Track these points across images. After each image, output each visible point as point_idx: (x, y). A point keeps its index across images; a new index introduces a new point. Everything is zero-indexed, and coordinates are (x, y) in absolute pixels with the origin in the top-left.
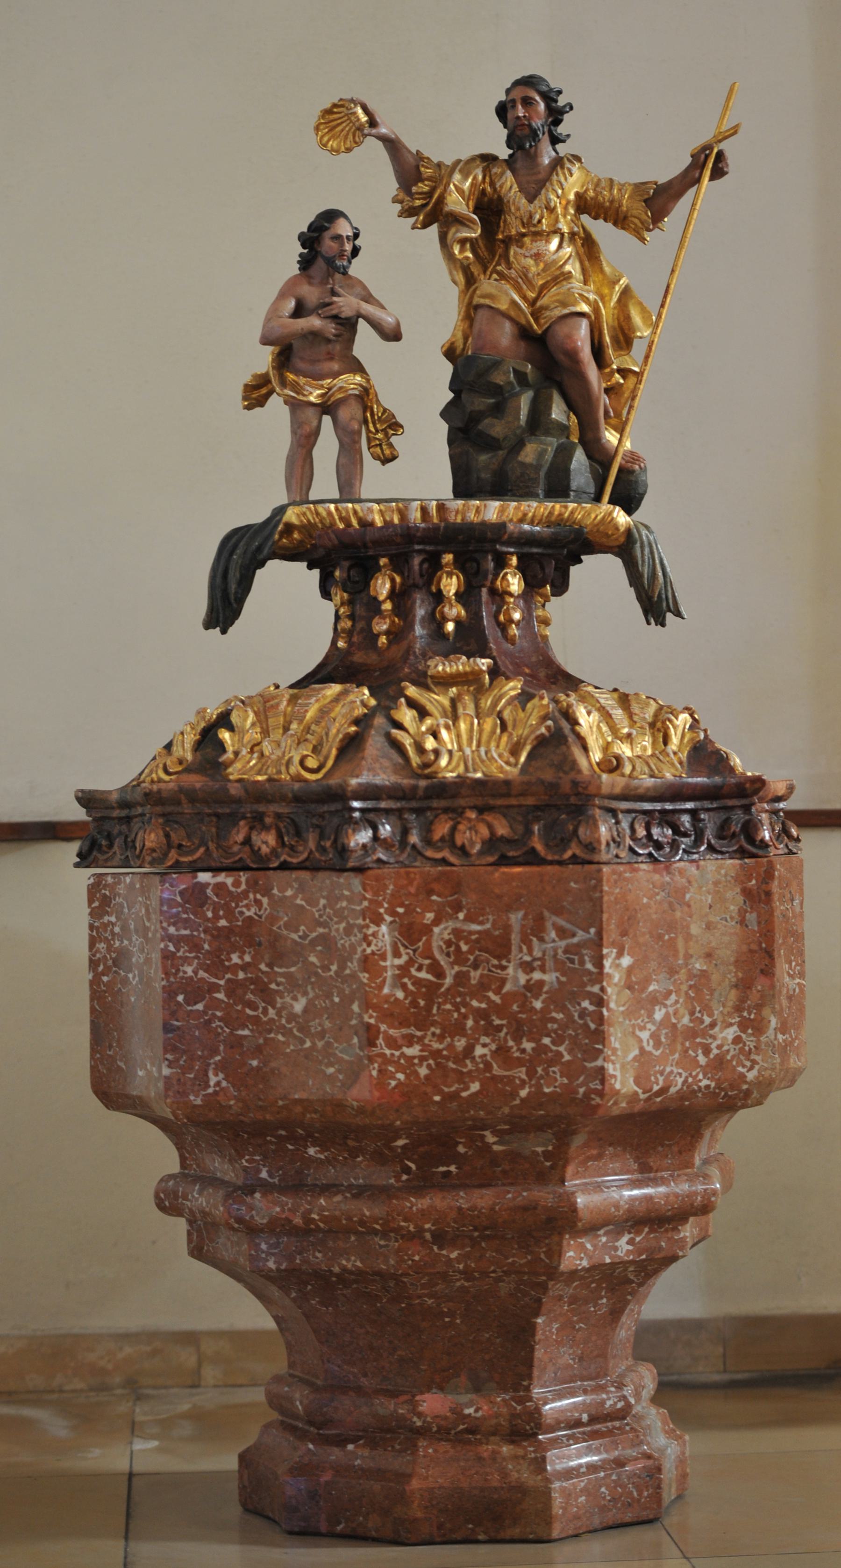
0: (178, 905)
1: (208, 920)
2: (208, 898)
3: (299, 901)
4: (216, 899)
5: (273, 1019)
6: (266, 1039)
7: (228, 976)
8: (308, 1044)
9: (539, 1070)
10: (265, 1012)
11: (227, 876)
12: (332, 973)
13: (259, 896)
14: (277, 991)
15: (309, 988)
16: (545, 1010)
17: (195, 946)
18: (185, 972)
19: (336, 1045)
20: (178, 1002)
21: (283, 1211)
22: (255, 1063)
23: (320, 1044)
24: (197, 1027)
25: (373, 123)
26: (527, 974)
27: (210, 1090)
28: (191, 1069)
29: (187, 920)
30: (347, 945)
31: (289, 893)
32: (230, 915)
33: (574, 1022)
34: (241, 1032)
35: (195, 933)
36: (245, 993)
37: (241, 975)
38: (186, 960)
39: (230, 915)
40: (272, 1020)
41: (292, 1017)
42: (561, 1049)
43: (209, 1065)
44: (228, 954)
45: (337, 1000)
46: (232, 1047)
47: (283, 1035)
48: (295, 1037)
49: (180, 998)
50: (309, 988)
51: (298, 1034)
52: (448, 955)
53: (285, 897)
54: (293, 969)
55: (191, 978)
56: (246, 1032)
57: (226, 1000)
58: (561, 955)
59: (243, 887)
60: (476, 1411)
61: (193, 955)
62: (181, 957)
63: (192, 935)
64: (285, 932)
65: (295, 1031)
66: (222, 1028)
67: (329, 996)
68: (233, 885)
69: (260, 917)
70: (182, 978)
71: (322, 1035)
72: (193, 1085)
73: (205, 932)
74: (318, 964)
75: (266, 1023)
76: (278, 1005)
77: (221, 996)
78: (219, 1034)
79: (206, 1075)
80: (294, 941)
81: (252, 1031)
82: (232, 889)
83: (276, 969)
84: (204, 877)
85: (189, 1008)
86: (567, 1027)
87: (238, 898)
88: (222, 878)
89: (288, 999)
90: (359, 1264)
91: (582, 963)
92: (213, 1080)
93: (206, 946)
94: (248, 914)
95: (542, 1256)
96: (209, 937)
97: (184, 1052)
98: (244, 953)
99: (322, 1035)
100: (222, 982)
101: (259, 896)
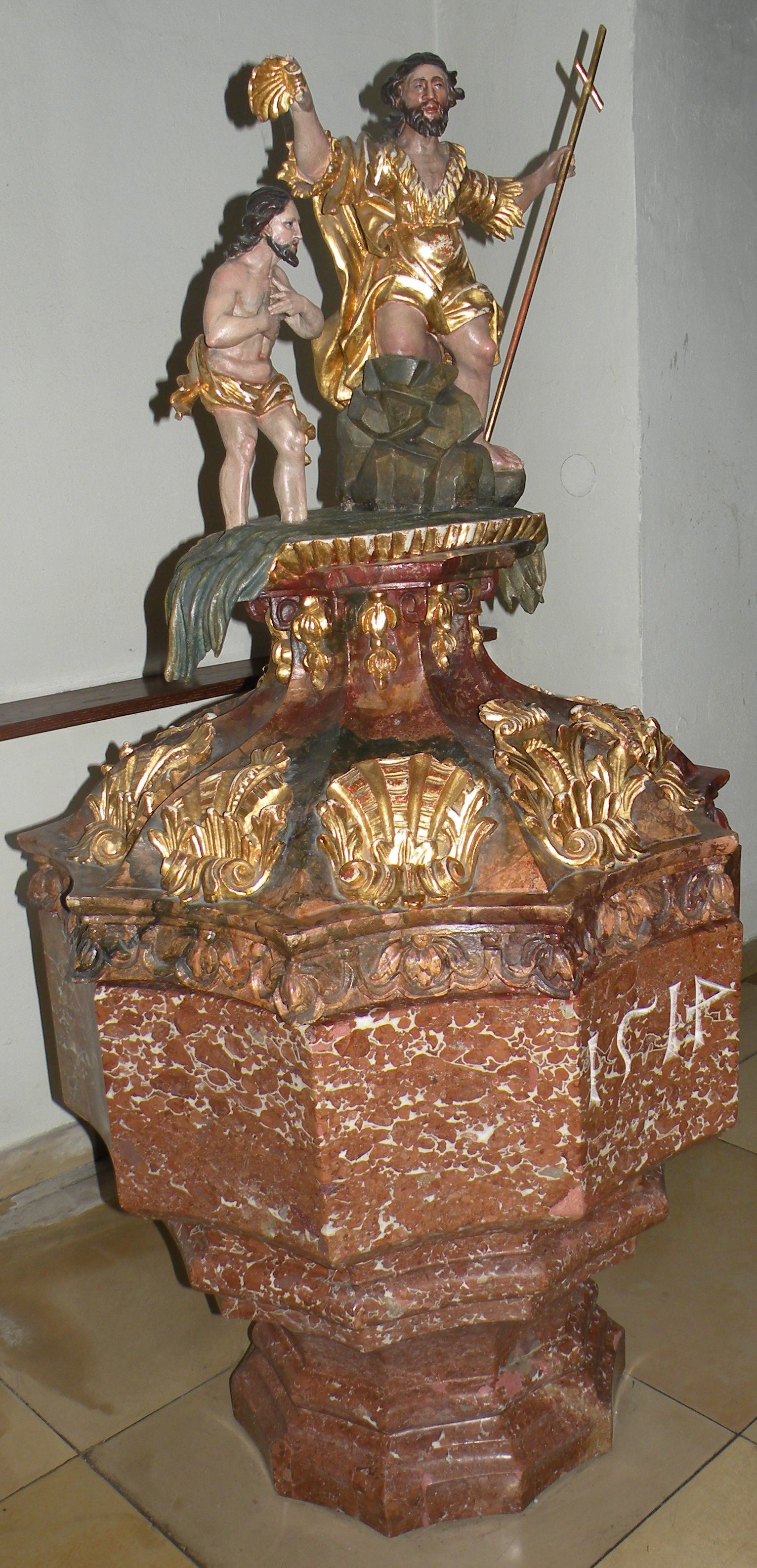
0: (336, 1059)
1: (371, 1067)
2: (369, 1044)
3: (484, 1032)
4: (379, 1044)
5: (452, 1153)
6: (443, 1174)
7: (398, 1119)
8: (497, 1170)
9: (689, 1122)
10: (442, 1147)
11: (391, 1017)
12: (530, 1099)
13: (432, 1033)
14: (457, 1125)
15: (498, 1117)
16: (695, 1067)
17: (356, 1097)
18: (346, 1128)
19: (534, 1168)
20: (341, 1160)
21: (420, 1303)
22: (431, 1199)
23: (512, 1169)
24: (363, 1179)
25: (241, 222)
26: (681, 1040)
27: (381, 1236)
28: (357, 1222)
29: (345, 1074)
30: (553, 1071)
31: (472, 1024)
32: (396, 1057)
33: (717, 1070)
34: (413, 1172)
35: (357, 1085)
36: (418, 1133)
37: (412, 1116)
38: (346, 1115)
39: (396, 1057)
40: (451, 1154)
41: (475, 1147)
42: (706, 1098)
43: (378, 1212)
44: (396, 1097)
45: (536, 1125)
46: (403, 1189)
47: (465, 1166)
48: (481, 1166)
49: (343, 1155)
50: (498, 1117)
51: (483, 1162)
52: (627, 1048)
53: (467, 1030)
54: (477, 1101)
55: (354, 1131)
56: (420, 1171)
57: (395, 1144)
58: (707, 1015)
59: (413, 1025)
60: (540, 1375)
61: (355, 1108)
62: (341, 1113)
63: (353, 1088)
64: (466, 1065)
65: (480, 1160)
66: (391, 1173)
67: (527, 1120)
68: (399, 1026)
69: (435, 1054)
70: (345, 1133)
71: (516, 1159)
72: (362, 1236)
73: (367, 1081)
74: (512, 1093)
75: (444, 1158)
76: (458, 1138)
77: (389, 1141)
78: (389, 1180)
79: (376, 1222)
80: (480, 1073)
81: (426, 1168)
82: (397, 1029)
83: (454, 1103)
84: (364, 1023)
85: (353, 1162)
86: (711, 1077)
87: (406, 1039)
88: (385, 1020)
89: (470, 1131)
90: (482, 1318)
91: (724, 1016)
92: (383, 1225)
93: (370, 1096)
94: (418, 1053)
95: (624, 1249)
96: (373, 1086)
97: (350, 1207)
98: (416, 1093)
99: (516, 1159)
100: (390, 1128)
101: (432, 1033)
